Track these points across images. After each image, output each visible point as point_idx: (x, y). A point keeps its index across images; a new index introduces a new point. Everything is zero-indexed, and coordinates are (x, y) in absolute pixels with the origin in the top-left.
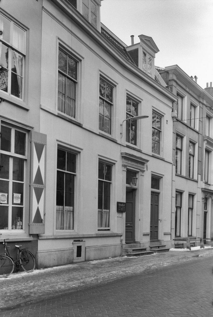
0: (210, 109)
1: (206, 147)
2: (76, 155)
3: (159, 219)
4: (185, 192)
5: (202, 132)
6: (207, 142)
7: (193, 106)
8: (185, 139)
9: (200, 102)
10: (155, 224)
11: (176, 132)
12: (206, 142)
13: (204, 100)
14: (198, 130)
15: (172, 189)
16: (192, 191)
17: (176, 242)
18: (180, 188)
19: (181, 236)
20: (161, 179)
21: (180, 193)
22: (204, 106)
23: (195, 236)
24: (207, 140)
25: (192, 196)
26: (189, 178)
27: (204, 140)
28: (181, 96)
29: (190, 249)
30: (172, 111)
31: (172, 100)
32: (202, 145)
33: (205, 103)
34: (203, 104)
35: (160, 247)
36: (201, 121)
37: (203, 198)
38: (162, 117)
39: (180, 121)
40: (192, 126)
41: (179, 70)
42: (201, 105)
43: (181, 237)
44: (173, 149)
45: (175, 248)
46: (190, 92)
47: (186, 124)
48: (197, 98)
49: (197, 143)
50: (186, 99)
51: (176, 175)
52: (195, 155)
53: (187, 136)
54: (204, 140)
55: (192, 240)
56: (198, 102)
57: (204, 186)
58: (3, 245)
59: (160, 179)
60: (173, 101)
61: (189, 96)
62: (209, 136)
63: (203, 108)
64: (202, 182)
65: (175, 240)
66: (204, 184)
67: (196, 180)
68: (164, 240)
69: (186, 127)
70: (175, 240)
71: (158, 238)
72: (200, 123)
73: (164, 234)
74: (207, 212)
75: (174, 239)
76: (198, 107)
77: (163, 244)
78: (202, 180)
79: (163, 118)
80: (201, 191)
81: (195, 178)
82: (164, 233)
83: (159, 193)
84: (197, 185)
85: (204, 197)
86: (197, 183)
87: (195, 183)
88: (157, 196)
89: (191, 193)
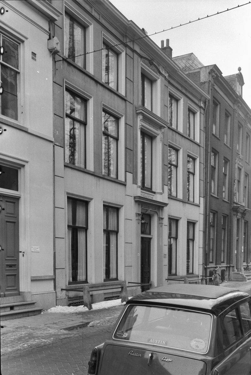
0: (150, 63)
1: (142, 125)
2: (18, 170)
3: (20, 251)
4: (93, 201)
5: (133, 100)
6: (143, 118)
7: (191, 112)
8: (91, 103)
9: (126, 46)
10: (6, 260)
11: (187, 153)
12: (140, 117)
13: (135, 44)
14: (199, 141)
15: (54, 191)
16: (193, 218)
17: (72, 294)
18: (175, 214)
19: (88, 281)
20: (22, 169)
21: (77, 203)
22: (135, 55)
23: (123, 280)
24: (141, 113)
25: (111, 209)
26: (105, 176)
27: (137, 113)
28: (83, 24)
29: (90, 308)
30: (50, 39)
31: (46, 16)
32: (135, 122)
33: (137, 48)
34: (134, 51)
35: (15, 308)
36: (202, 130)
37: (139, 214)
38: (20, 44)
39: (102, 85)
40: (192, 137)
41: (152, 45)
42: (129, 52)
43: (88, 283)
44: (54, 114)
45: (69, 305)
46: (100, 21)
47: (182, 135)
48: (121, 38)
49: (122, 116)
50: (181, 102)
51: (169, 198)
52: (196, 173)
53: (183, 149)
54: (138, 114)
55: (94, 289)
56: (123, 46)
57: (139, 192)
58: (156, 287)
59: (20, 168)
60: (51, 21)
61: (99, 27)
62: (152, 110)
63: (133, 59)
64: (135, 186)
65: (67, 290)
66: (139, 190)
67: (181, 199)
68: (32, 292)
69: (93, 83)
70: (67, 290)
71: (18, 289)
72: (127, 83)
73: (32, 280)
74: (152, 238)
75: (64, 288)
76: (123, 54)
77: (29, 300)
78: (135, 182)
79: (21, 44)
80: (133, 201)
81: (121, 178)
82: (32, 277)
83: (17, 199)
84: (125, 190)
85: (140, 213)
86: (125, 187)
87: (120, 188)
88: (14, 203)
89: (72, 194)
